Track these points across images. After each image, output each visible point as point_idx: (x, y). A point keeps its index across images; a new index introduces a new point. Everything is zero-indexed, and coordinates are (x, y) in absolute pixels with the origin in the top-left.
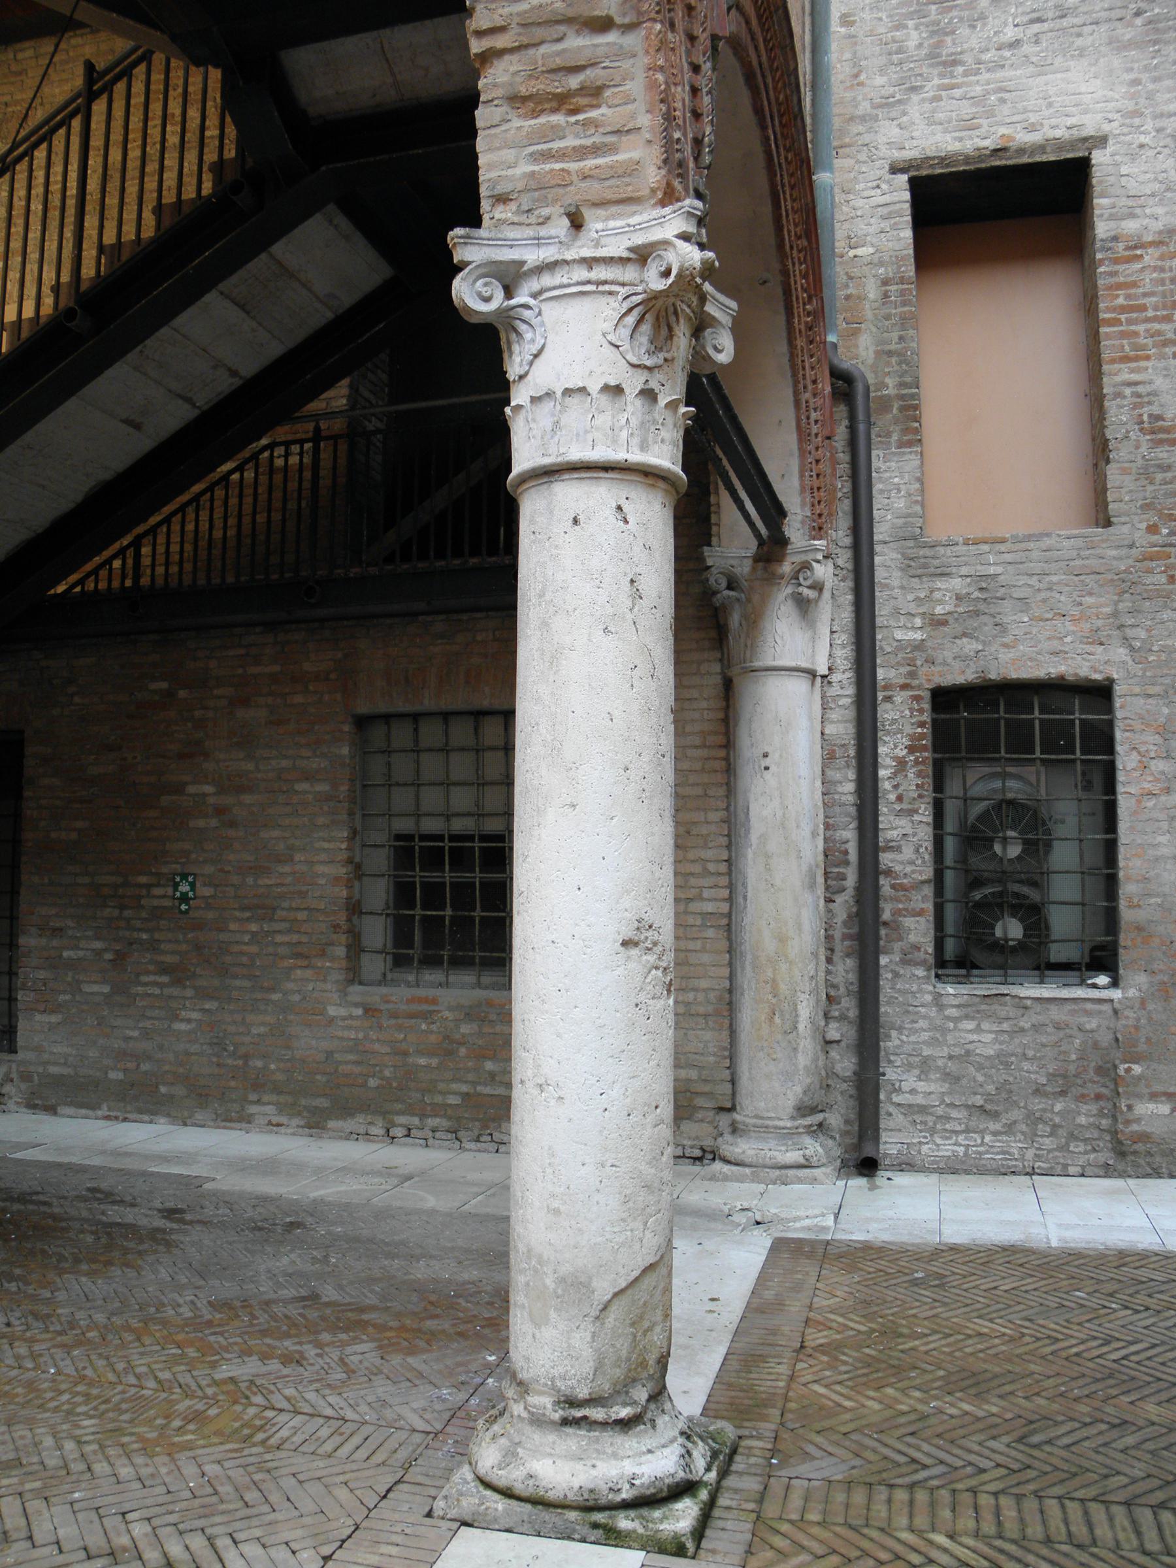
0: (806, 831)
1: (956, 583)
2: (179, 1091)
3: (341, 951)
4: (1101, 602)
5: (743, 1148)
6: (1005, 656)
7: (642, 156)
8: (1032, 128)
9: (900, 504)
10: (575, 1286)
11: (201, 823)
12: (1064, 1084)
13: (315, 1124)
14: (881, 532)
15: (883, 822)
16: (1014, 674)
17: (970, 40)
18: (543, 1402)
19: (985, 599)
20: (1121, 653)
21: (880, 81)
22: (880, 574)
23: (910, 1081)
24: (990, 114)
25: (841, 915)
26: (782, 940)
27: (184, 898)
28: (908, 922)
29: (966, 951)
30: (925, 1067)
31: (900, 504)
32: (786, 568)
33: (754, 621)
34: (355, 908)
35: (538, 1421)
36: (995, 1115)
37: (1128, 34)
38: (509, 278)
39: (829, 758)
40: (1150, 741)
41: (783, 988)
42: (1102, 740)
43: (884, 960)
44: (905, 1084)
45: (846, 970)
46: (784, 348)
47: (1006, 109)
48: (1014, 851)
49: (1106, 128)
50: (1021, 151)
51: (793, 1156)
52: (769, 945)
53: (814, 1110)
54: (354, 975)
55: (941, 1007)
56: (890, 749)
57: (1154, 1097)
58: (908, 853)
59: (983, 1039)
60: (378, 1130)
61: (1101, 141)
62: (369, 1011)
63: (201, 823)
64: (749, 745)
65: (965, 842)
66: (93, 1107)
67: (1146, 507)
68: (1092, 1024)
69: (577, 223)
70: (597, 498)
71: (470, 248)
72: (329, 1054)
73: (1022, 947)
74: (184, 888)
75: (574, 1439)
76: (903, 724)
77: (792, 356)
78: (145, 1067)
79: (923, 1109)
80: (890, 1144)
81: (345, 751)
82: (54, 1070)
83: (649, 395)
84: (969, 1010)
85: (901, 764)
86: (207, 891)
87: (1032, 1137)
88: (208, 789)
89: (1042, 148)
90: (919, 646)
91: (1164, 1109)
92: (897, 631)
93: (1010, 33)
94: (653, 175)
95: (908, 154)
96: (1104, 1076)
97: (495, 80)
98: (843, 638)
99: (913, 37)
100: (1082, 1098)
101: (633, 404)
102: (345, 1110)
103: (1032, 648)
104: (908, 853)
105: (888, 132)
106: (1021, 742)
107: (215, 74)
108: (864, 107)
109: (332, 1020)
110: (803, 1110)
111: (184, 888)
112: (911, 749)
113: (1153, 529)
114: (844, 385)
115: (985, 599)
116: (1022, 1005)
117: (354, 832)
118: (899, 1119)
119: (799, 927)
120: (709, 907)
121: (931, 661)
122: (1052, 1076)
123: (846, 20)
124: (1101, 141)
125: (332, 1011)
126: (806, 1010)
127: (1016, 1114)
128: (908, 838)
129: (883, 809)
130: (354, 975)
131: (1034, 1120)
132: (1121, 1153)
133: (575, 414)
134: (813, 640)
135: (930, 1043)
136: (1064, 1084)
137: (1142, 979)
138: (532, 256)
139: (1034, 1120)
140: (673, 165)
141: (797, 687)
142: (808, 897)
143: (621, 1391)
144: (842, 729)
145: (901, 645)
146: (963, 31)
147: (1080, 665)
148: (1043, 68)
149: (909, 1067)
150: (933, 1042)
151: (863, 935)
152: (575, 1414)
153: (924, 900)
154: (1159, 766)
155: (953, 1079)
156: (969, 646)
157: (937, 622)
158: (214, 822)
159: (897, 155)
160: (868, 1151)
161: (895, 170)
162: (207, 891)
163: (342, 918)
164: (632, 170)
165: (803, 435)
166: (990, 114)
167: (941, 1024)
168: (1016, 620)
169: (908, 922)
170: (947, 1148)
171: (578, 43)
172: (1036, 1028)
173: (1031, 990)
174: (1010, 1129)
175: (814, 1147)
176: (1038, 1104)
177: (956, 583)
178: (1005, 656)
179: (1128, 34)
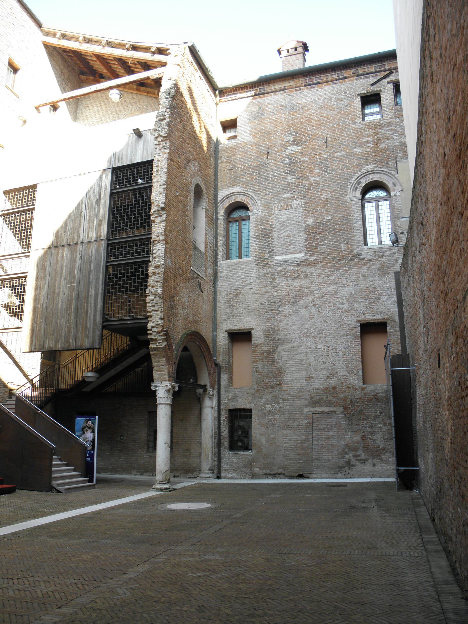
0: (210, 430)
1: (232, 394)
2: (121, 470)
3: (146, 447)
4: (250, 398)
5: (201, 475)
6: (238, 405)
7: (166, 377)
8: (244, 326)
9: (225, 382)
10: (161, 472)
11: (124, 427)
12: (246, 466)
13: (142, 474)
14: (222, 386)
15: (221, 428)
16: (239, 408)
17: (236, 312)
18: (158, 482)
19: (235, 397)
20: (253, 405)
21: (224, 317)
22: (221, 393)
23: (225, 466)
24: (238, 323)
25: (216, 442)
26: (206, 445)
27: (122, 439)
28: (225, 443)
29: (232, 447)
30: (227, 464)
31: (225, 382)
32: (207, 393)
33: (203, 400)
34: (148, 441)
35: (158, 483)
36: (237, 471)
37: (257, 313)
38: (156, 387)
39: (215, 419)
40: (256, 417)
41: (207, 452)
42: (250, 417)
43: (221, 448)
44: (225, 466)
45: (216, 450)
46: (205, 363)
47: (241, 323)
48: (240, 433)
49: (254, 327)
50: (242, 330)
51: (207, 476)
52: (205, 446)
53: (212, 470)
54: (148, 451)
55: (229, 455)
56: (222, 418)
57: (257, 468)
58: (225, 433)
59: (235, 460)
60: (151, 475)
61: (253, 329)
62: (150, 456)
63: (124, 427)
64: (202, 419)
65: (232, 431)
66: (106, 473)
67: (257, 384)
68: (249, 457)
69: (161, 382)
70: (163, 406)
71: (153, 384)
72: (144, 463)
73: (242, 447)
74: (122, 437)
75: (160, 485)
76: (224, 415)
77: (206, 364)
78: (115, 466)
79: (227, 470)
80: (223, 475)
81: (147, 417)
82: (100, 467)
83: (167, 397)
84: (233, 455)
85: (224, 420)
86: (125, 438)
87: (241, 474)
88: (126, 422)
89: (245, 329)
90: (227, 403)
91: (258, 469)
92: (224, 401)
93: (241, 312)
94: (167, 379)
95: (228, 329)
96: (250, 464)
97: (155, 369)
98: (217, 402)
99: (229, 311)
100: (248, 468)
101: (166, 398)
102: (146, 472)
103: (241, 404)
104: (225, 433)
105: (225, 325)
106: (241, 417)
107: (128, 337)
108: (222, 321)
109: (144, 458)
110: (209, 470)
111: (122, 437)
112: (225, 418)
113: (257, 387)
114: (216, 365)
115: (235, 397)
116: (240, 455)
117: (148, 429)
118: (224, 471)
119: (209, 443)
120: (198, 441)
121: (228, 405)
122: (244, 465)
123: (219, 307)
124: (253, 329)
125: (145, 456)
126: (210, 455)
127: (239, 471)
128: (225, 431)
129: (221, 427)
130: (148, 451)
131: (242, 471)
132: (253, 476)
133: (161, 399)
134: (212, 402)
135: (228, 460)
136: (246, 466)
137: (255, 451)
138: (158, 385)
139: (242, 471)
140: (170, 376)
141: (209, 409)
142: (211, 439)
143: (165, 481)
144: (216, 415)
145: (224, 403)
146: (235, 310)
147: (247, 406)
148: (246, 317)
149: (225, 464)
150: (228, 460)
151: (219, 445)
152: (160, 483)
153: (227, 440)
154: (257, 421)
155: (231, 465)
156: (233, 403)
157: (229, 400)
158: (127, 427)
159: (226, 329)
160: (219, 476)
161: (226, 331)
162: (125, 438)
163: (146, 442)
164: (166, 378)
165: (209, 374)
166: (238, 323)
167: (230, 458)
168: (240, 400)
169: (225, 443)
170: (230, 475)
171: (161, 367)
172: (242, 458)
173: (241, 453)
174: (239, 473)
175: (211, 475)
176: (242, 469)
177: (232, 394)
178: (238, 405)
179: (257, 313)
